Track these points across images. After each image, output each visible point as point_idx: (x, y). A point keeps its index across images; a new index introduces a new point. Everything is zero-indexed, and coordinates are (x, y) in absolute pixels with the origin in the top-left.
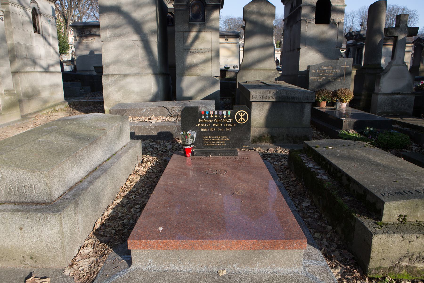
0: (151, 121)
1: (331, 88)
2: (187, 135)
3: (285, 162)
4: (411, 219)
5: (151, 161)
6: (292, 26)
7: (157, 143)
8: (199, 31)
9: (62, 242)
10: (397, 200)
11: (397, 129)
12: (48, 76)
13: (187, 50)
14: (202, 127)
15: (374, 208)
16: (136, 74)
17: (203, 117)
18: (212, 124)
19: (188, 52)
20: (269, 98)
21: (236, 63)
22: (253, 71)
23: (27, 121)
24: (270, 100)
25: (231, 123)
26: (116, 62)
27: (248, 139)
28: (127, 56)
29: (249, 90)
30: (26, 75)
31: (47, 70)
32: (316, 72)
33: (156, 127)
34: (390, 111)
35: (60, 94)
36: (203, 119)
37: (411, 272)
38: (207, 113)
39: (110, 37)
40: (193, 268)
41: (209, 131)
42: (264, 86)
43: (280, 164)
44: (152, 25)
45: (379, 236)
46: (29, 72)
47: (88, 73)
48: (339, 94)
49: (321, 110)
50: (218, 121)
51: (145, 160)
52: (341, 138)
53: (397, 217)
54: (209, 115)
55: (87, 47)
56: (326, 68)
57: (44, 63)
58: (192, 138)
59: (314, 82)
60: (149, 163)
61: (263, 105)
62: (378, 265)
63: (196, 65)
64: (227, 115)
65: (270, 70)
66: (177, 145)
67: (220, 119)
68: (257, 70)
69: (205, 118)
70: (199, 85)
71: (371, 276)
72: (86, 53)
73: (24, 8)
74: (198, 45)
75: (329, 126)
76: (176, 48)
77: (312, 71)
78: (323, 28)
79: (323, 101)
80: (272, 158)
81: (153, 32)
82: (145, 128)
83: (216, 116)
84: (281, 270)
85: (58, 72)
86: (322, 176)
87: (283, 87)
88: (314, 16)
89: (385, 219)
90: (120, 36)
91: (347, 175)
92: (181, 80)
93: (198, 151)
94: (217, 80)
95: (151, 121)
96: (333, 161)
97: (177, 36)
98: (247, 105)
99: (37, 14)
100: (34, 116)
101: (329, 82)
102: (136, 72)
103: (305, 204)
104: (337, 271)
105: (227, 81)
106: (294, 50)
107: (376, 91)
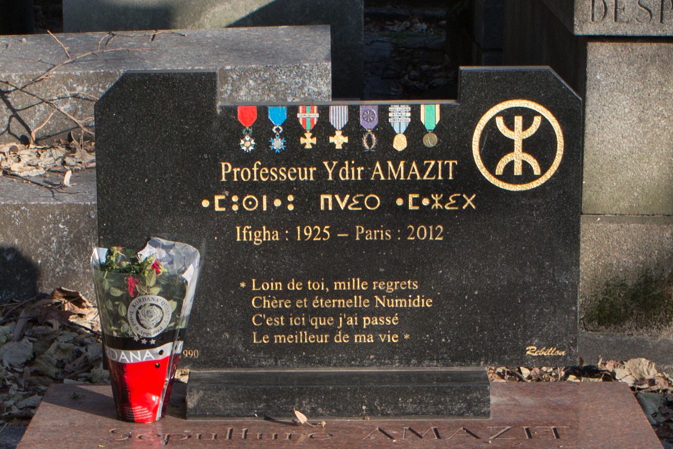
2: (137, 270)
14: (243, 217)
17: (247, 144)
18: (307, 195)
27: (561, 297)
36: (245, 160)
38: (277, 117)
41: (291, 245)
50: (351, 173)
54: (293, 129)
58: (173, 289)
64: (415, 129)
66: (65, 339)
67: (366, 160)
69: (263, 153)
83: (339, 140)
93: (213, 384)
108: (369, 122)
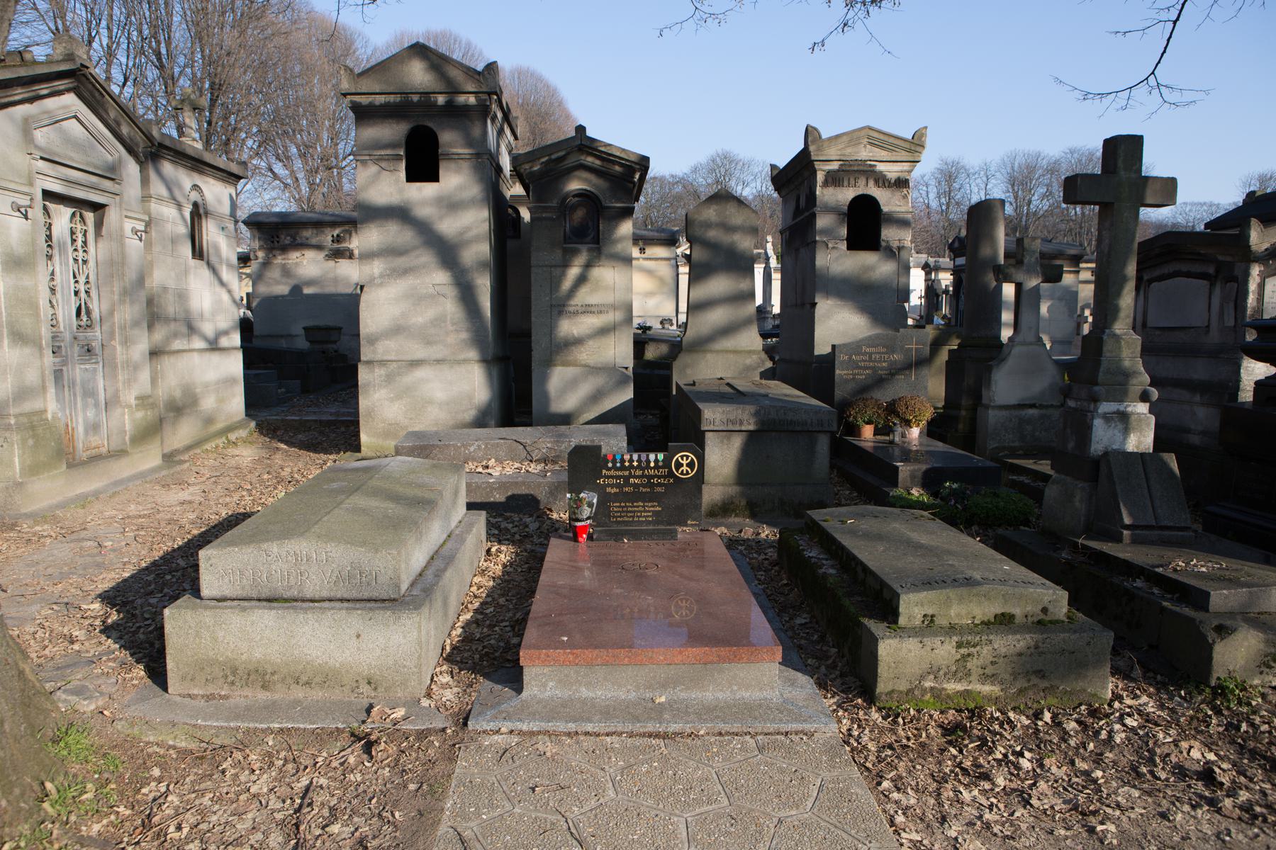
0: (489, 471)
1: (884, 396)
2: (581, 500)
3: (772, 554)
4: (941, 621)
5: (505, 554)
6: (797, 250)
7: (506, 519)
8: (588, 266)
9: (419, 657)
10: (919, 591)
11: (1014, 484)
12: (215, 358)
13: (559, 308)
14: (609, 485)
15: (886, 608)
16: (439, 361)
17: (610, 465)
18: (627, 479)
19: (560, 313)
20: (741, 423)
21: (668, 309)
22: (709, 356)
23: (178, 468)
24: (743, 428)
25: (665, 477)
26: (397, 330)
27: (698, 507)
28: (420, 318)
29: (701, 405)
30: (172, 359)
31: (214, 346)
32: (850, 358)
33: (502, 485)
34: (1017, 444)
35: (236, 403)
36: (609, 469)
37: (938, 697)
38: (618, 457)
39: (382, 276)
40: (615, 694)
41: (622, 493)
42: (733, 396)
43: (763, 557)
44: (479, 250)
45: (888, 641)
46: (178, 352)
47: (283, 344)
48: (901, 409)
49: (862, 444)
50: (639, 473)
51: (493, 550)
52: (893, 505)
53: (920, 617)
54: (623, 461)
55: (286, 272)
56: (873, 350)
57: (208, 329)
58: (590, 505)
59: (847, 381)
60: (502, 556)
61: (729, 439)
62: (890, 688)
63: (578, 341)
64: (656, 461)
65: (750, 352)
66: (548, 522)
67: (643, 469)
68: (718, 352)
69: (614, 467)
70: (585, 389)
71: (882, 705)
72: (283, 289)
73: (179, 206)
74: (585, 296)
75: (869, 479)
76: (533, 303)
77: (841, 358)
78: (868, 258)
79: (868, 423)
80: (749, 548)
81: (482, 265)
82: (478, 487)
83: (635, 464)
84: (747, 695)
85: (236, 348)
86: (829, 569)
87: (773, 399)
88: (844, 232)
89: (902, 621)
90: (405, 272)
91: (862, 563)
92: (545, 378)
93: (601, 532)
94: (628, 377)
95: (489, 471)
96: (847, 542)
97: (537, 276)
98: (696, 440)
99: (200, 216)
100: (186, 457)
101: (879, 382)
102: (439, 356)
103: (799, 621)
104: (832, 701)
105: (648, 371)
106: (803, 305)
107: (985, 401)
108: (643, 459)
